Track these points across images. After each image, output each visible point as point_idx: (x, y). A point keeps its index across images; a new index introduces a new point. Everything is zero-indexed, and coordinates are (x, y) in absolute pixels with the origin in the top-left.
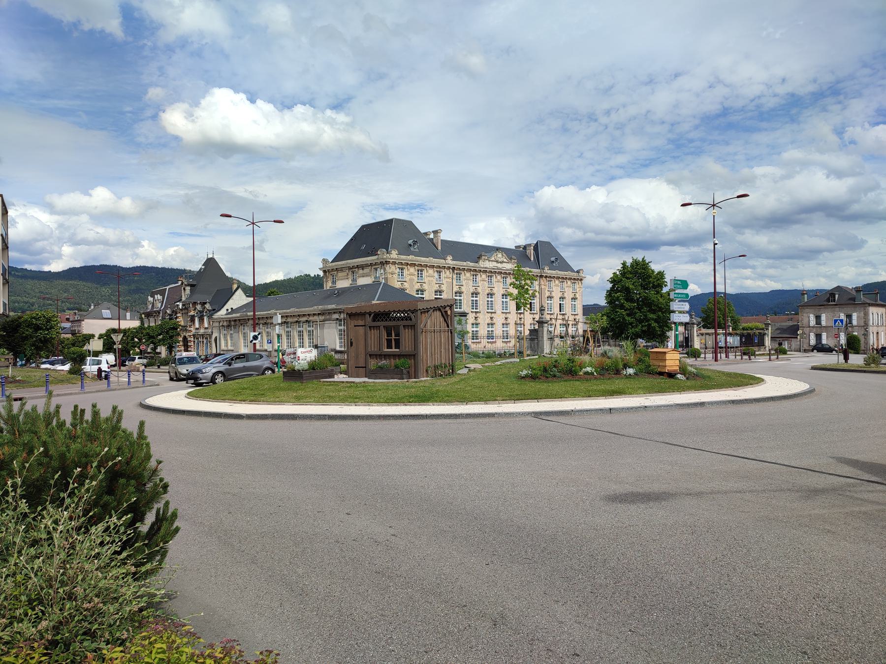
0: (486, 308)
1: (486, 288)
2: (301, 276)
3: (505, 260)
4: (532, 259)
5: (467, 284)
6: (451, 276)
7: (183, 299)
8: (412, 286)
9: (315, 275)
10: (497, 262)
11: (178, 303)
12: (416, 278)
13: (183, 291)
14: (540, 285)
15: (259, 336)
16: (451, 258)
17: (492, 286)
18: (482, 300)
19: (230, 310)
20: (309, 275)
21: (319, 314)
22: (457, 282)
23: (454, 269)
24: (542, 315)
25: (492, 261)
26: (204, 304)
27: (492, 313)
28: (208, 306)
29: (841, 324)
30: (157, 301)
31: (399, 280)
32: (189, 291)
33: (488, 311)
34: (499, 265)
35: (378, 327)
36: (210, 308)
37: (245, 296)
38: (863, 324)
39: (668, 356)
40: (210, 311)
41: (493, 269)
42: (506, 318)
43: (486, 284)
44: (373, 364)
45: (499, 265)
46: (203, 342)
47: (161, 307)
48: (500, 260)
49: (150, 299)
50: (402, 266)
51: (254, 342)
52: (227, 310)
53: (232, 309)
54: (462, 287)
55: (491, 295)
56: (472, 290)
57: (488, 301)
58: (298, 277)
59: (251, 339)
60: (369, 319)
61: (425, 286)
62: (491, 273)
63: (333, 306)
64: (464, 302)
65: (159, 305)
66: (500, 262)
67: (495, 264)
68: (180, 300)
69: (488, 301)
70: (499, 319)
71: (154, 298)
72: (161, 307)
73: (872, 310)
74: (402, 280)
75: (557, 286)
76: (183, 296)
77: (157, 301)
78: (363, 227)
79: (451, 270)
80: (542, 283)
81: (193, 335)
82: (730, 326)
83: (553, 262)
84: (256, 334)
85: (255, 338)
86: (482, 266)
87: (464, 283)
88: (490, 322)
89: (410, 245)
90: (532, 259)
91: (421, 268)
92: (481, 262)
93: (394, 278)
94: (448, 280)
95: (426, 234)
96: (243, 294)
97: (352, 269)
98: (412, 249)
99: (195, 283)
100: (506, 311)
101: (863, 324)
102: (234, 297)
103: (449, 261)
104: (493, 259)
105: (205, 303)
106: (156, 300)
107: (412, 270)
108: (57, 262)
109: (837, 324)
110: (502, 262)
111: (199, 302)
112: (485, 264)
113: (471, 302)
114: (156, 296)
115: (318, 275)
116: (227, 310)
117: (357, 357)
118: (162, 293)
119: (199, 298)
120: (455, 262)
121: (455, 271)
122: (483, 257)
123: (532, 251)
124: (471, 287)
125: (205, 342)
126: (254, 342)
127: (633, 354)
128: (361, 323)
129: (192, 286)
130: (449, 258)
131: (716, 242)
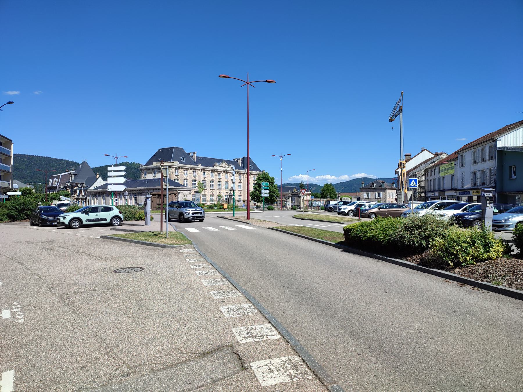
0: (217, 188)
1: (217, 178)
2: (123, 163)
3: (227, 166)
4: (240, 165)
5: (208, 177)
6: (200, 173)
7: (71, 181)
8: (182, 178)
9: (132, 163)
10: (223, 167)
11: (68, 183)
12: (183, 174)
13: (70, 177)
14: (243, 177)
15: (118, 200)
16: (201, 165)
17: (220, 178)
18: (215, 184)
19: (96, 187)
20: (128, 163)
21: (139, 190)
22: (203, 176)
23: (202, 170)
24: (230, 192)
25: (220, 166)
26: (82, 184)
27: (220, 190)
28: (84, 185)
29: (415, 184)
30: (55, 182)
31: (176, 175)
32: (74, 177)
33: (218, 189)
34: (224, 168)
35: (159, 198)
36: (86, 186)
37: (102, 181)
38: (384, 197)
39: (224, 205)
40: (85, 187)
41: (221, 170)
42: (240, 193)
43: (218, 177)
44: (157, 206)
45: (224, 168)
46: (81, 202)
47: (57, 185)
48: (224, 166)
49: (51, 180)
50: (177, 169)
51: (116, 201)
52: (95, 187)
53: (97, 187)
54: (206, 178)
55: (220, 182)
56: (211, 179)
57: (218, 185)
58: (121, 163)
59: (115, 200)
60: (157, 196)
61: (188, 178)
62: (220, 172)
63: (146, 188)
64: (207, 185)
65: (56, 183)
66: (224, 167)
67: (222, 168)
68: (69, 182)
69: (218, 185)
70: (216, 193)
71: (53, 180)
72: (57, 185)
73: (388, 191)
74: (177, 175)
75: (252, 178)
76: (71, 180)
77: (55, 182)
78: (160, 149)
79: (200, 170)
80: (245, 176)
81: (76, 199)
82: (328, 197)
83: (251, 167)
84: (117, 198)
85: (116, 200)
86: (216, 169)
87: (207, 176)
88: (212, 194)
89: (182, 159)
90: (240, 165)
91: (186, 169)
92: (215, 167)
93: (173, 174)
94: (199, 175)
95: (189, 154)
96: (102, 180)
97: (154, 169)
98: (182, 161)
99: (76, 173)
100: (227, 189)
101: (384, 197)
102: (98, 181)
103: (200, 166)
104: (221, 165)
105: (83, 183)
106: (54, 181)
107: (182, 170)
108: (278, 233)
109: (412, 184)
110: (225, 167)
111: (79, 183)
112: (216, 168)
113: (210, 185)
114: (54, 179)
115: (134, 163)
116: (95, 187)
117: (154, 205)
118: (58, 177)
119: (79, 181)
120: (202, 167)
121: (203, 171)
122: (216, 165)
123: (241, 162)
124: (210, 178)
125: (82, 202)
126: (116, 201)
127: (413, 219)
128: (155, 197)
129: (75, 175)
130: (200, 165)
131: (282, 169)
